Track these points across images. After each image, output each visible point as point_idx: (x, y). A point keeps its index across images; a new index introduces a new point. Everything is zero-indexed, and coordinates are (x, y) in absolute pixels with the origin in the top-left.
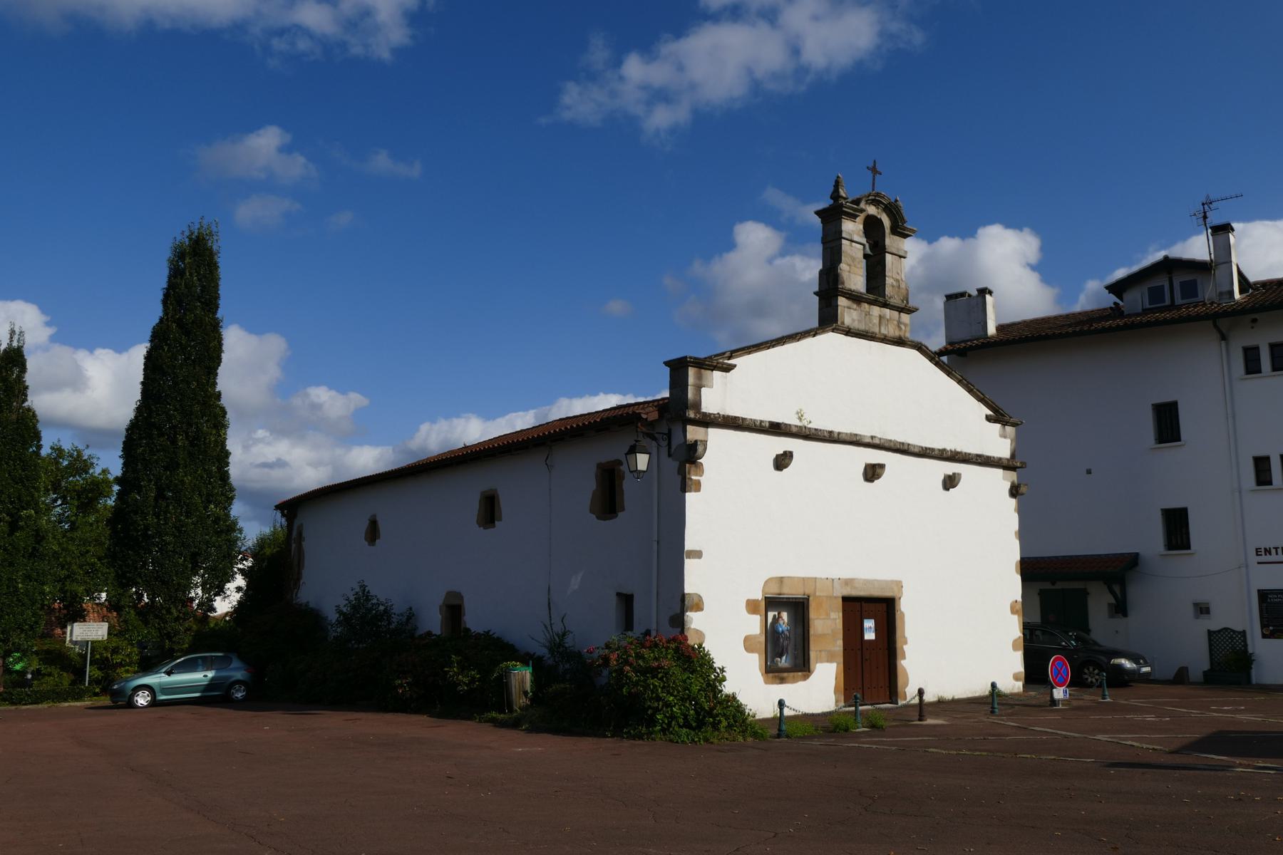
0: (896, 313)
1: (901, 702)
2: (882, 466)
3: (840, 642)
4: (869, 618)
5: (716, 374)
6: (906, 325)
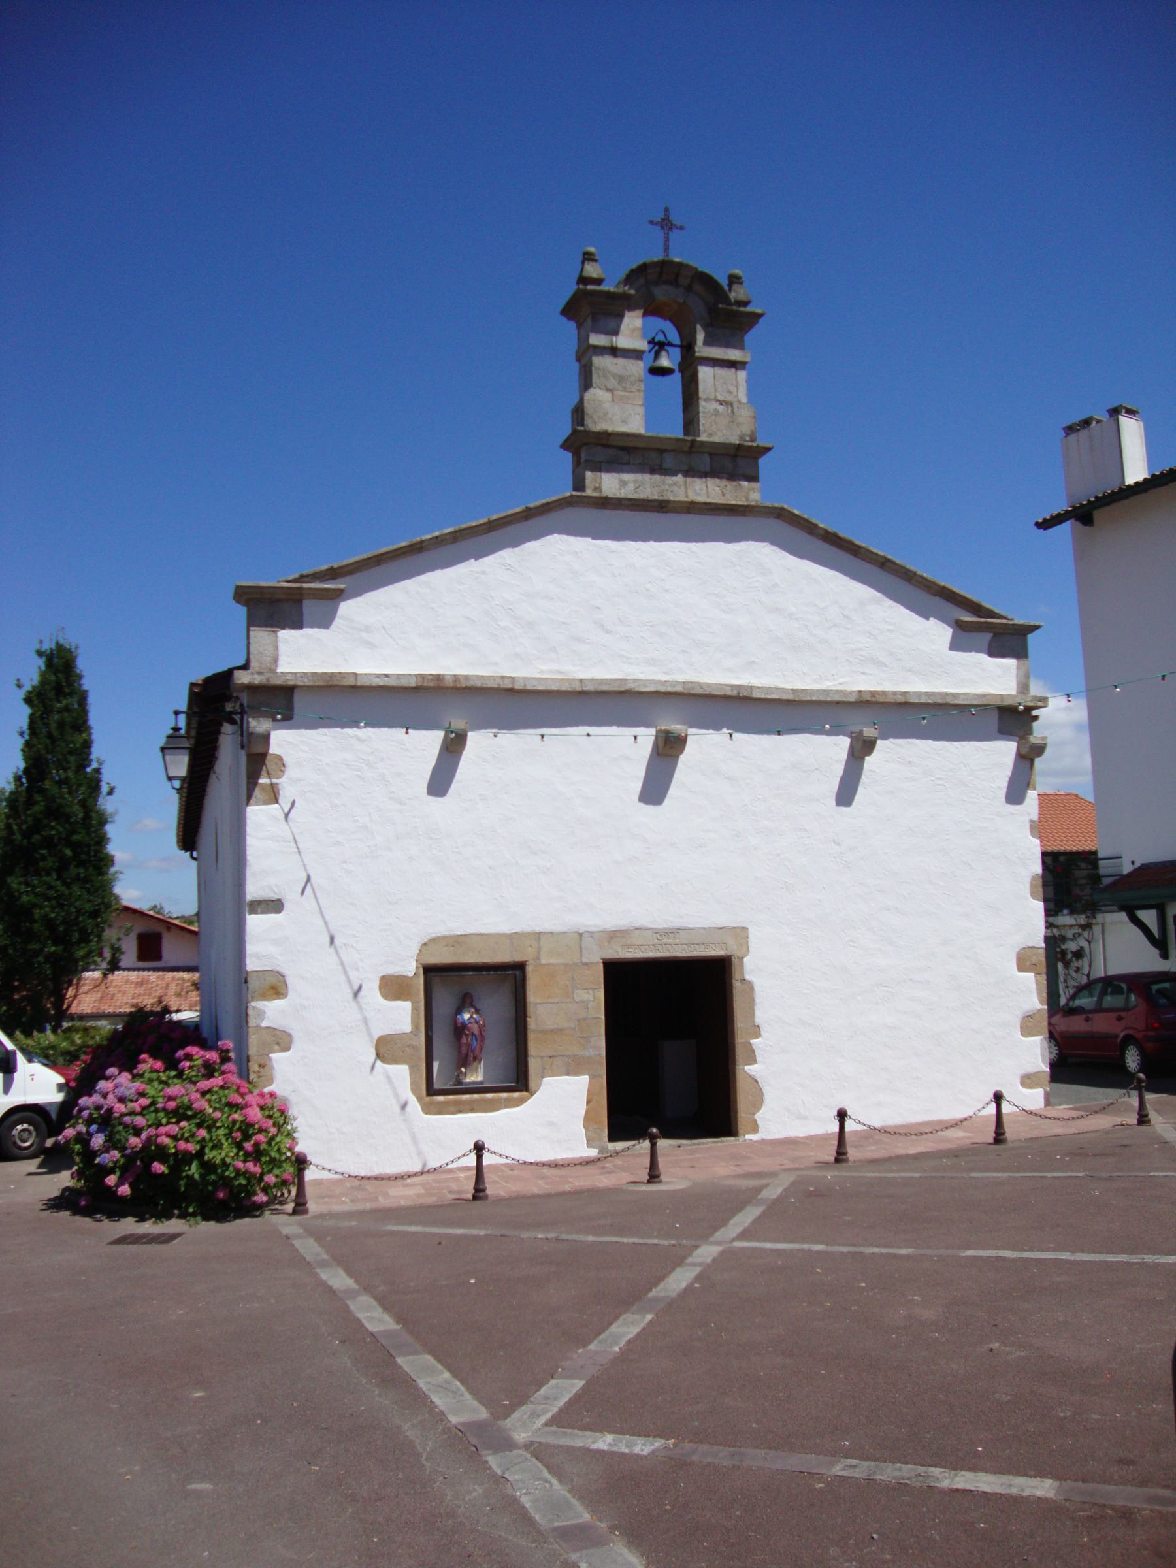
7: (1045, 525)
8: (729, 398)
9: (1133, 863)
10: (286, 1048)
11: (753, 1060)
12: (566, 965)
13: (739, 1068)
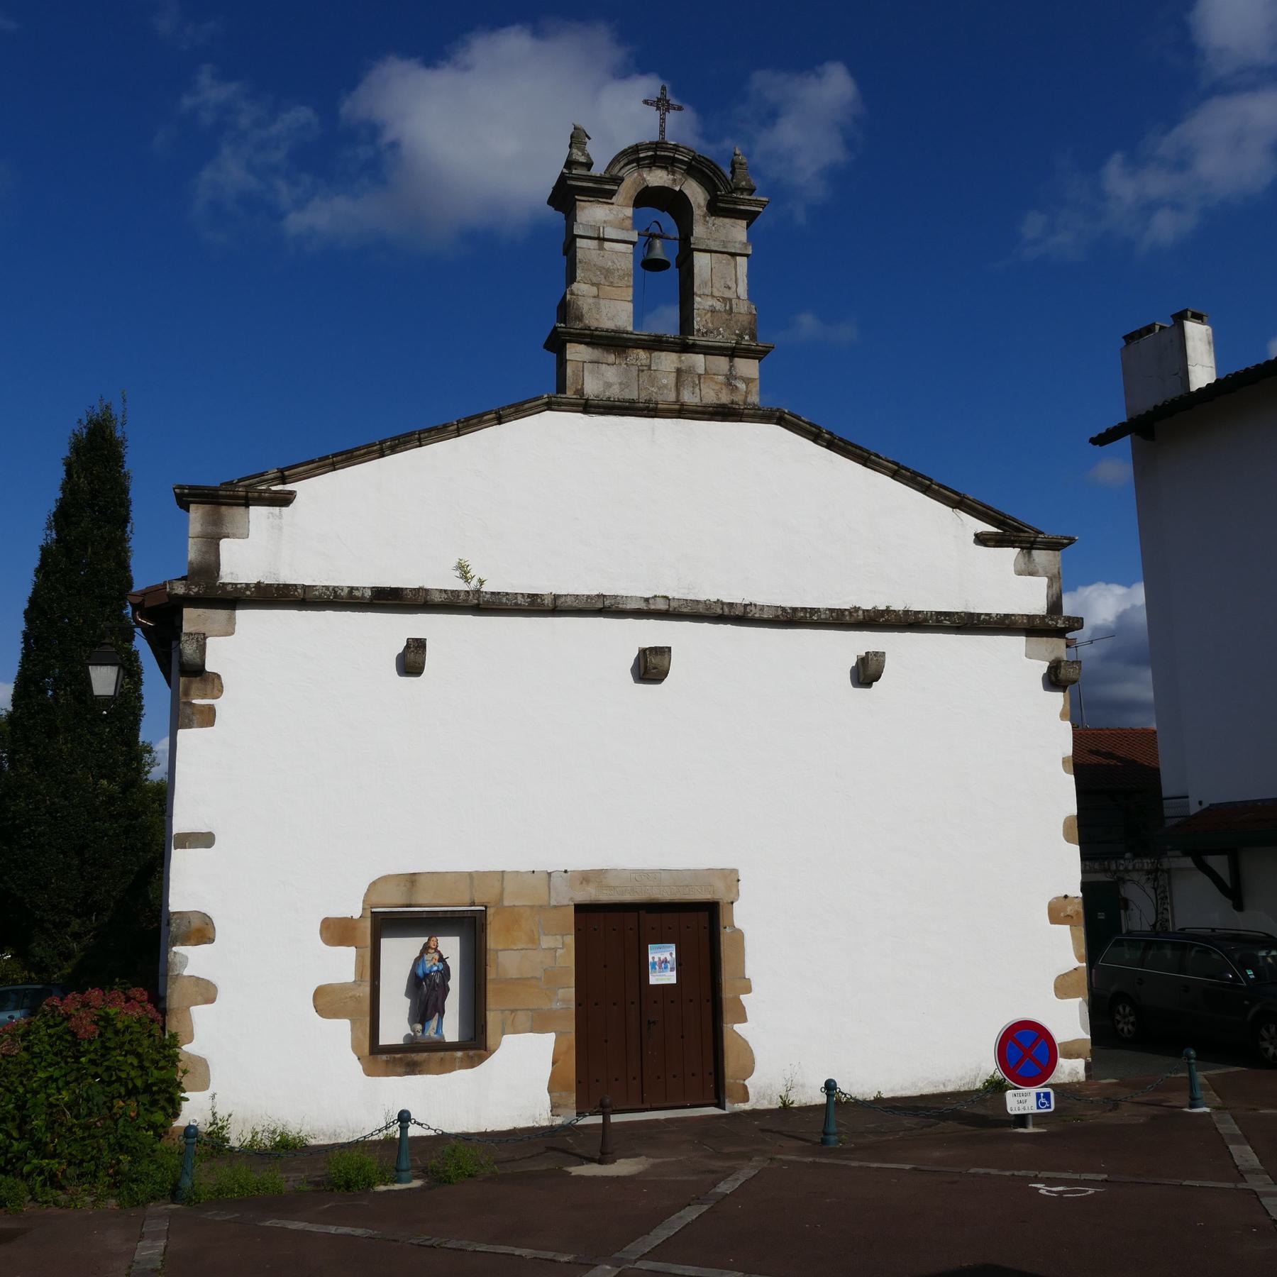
0: (721, 363)
1: (733, 1107)
2: (664, 652)
3: (571, 992)
4: (662, 940)
5: (256, 512)
6: (748, 381)
7: (1102, 440)
8: (728, 294)
9: (1200, 803)
10: (210, 999)
11: (743, 1019)
12: (532, 907)
13: (726, 1027)
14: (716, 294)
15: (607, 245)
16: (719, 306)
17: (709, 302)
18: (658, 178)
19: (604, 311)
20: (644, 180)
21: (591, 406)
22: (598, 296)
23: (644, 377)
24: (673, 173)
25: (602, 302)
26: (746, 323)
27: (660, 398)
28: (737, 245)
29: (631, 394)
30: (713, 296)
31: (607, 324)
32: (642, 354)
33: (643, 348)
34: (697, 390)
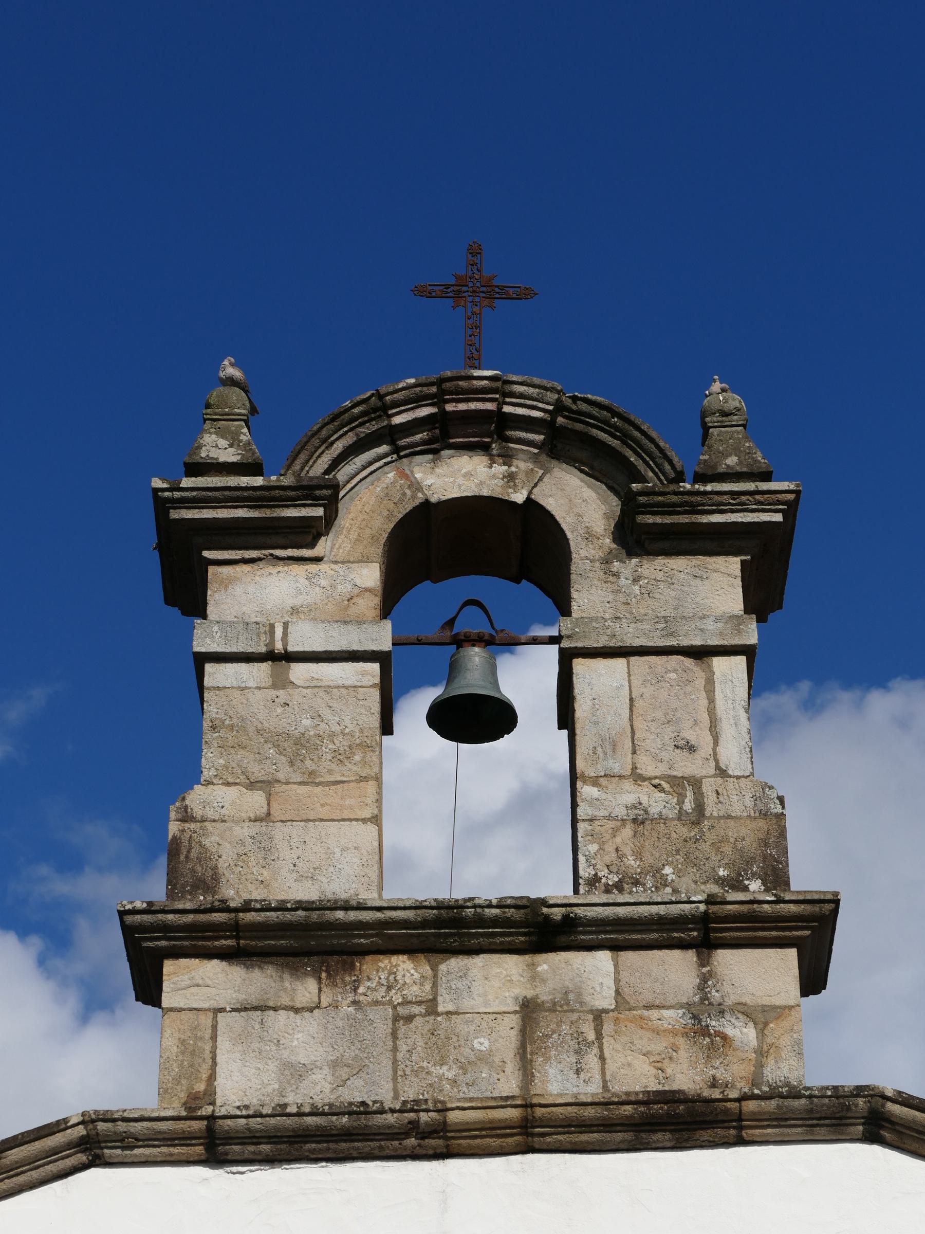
0: (674, 970)
8: (686, 766)
14: (648, 768)
15: (299, 672)
16: (658, 803)
17: (629, 795)
18: (460, 476)
19: (286, 855)
20: (416, 486)
21: (231, 1138)
22: (267, 817)
23: (415, 1035)
24: (507, 458)
25: (279, 831)
26: (750, 844)
27: (449, 1094)
28: (710, 625)
29: (376, 1087)
30: (637, 777)
31: (291, 887)
32: (407, 971)
33: (410, 950)
34: (591, 1060)
